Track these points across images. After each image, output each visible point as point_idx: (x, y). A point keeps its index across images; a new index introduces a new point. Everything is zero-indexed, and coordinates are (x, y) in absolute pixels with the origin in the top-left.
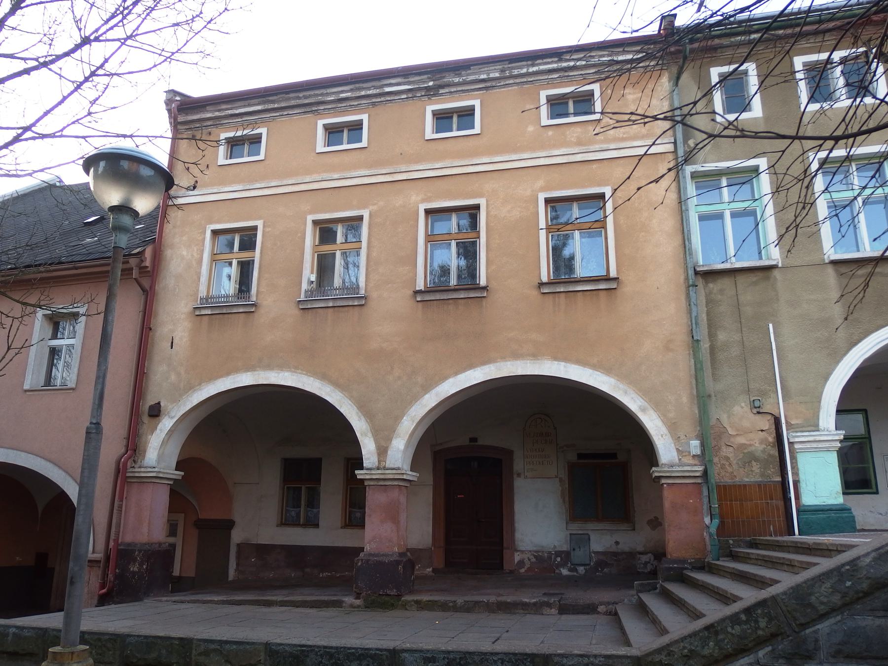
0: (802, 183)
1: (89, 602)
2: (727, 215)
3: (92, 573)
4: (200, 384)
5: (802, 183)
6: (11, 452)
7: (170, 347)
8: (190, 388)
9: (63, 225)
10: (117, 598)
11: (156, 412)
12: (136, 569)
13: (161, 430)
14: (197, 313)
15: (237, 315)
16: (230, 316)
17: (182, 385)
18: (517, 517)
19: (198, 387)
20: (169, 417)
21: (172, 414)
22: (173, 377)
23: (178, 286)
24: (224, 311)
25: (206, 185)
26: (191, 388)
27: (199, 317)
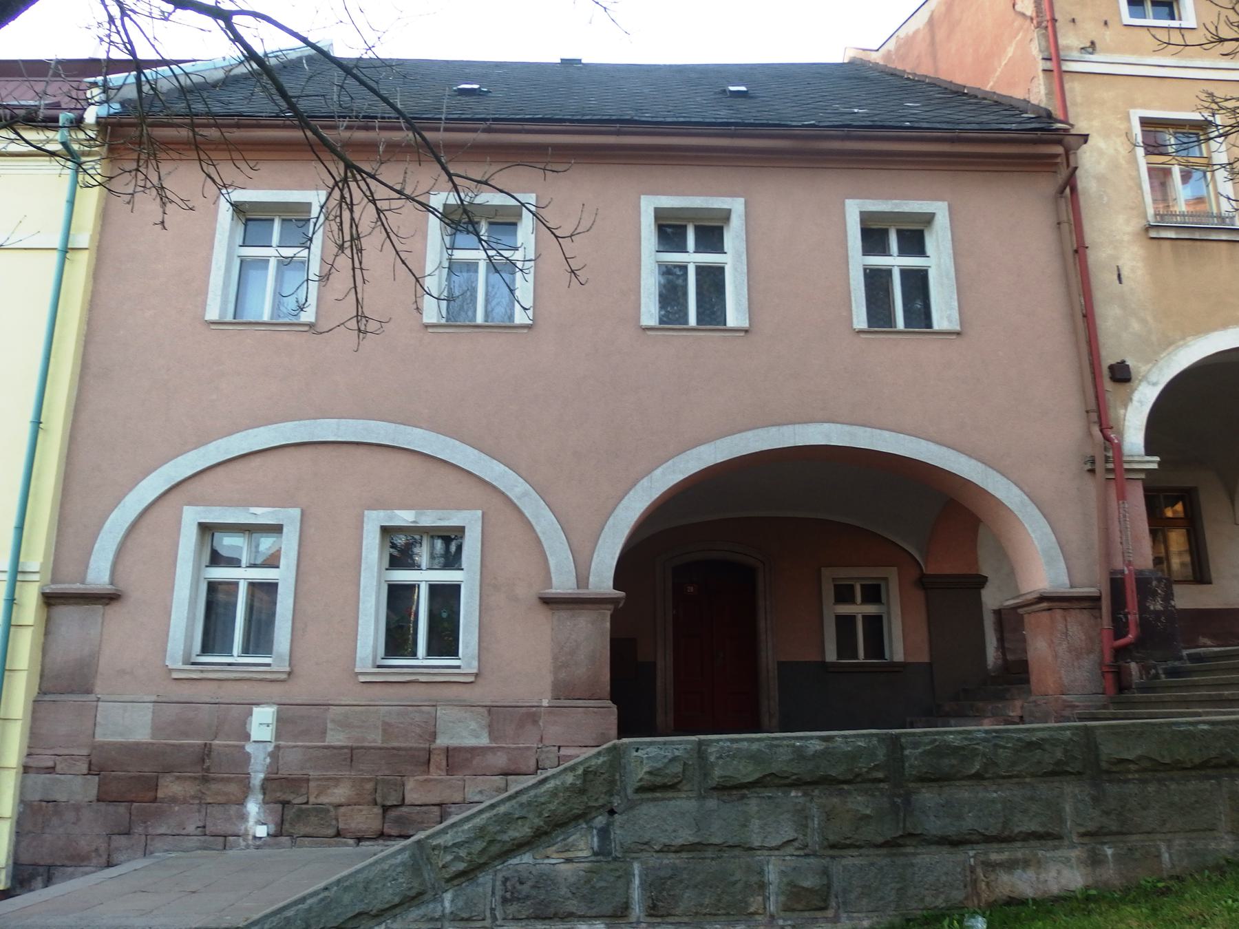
0: (576, 229)
1: (1076, 664)
2: (273, 264)
3: (1069, 619)
4: (1183, 338)
5: (576, 229)
6: (859, 431)
7: (1117, 282)
8: (1169, 343)
9: (490, 94)
10: (1138, 652)
11: (1122, 375)
12: (1159, 607)
13: (1140, 402)
14: (1153, 234)
15: (1215, 244)
16: (1205, 244)
17: (1154, 338)
18: (1207, 535)
19: (1181, 343)
20: (1149, 383)
21: (1153, 378)
22: (1136, 326)
23: (1104, 192)
24: (1197, 236)
25: (1108, 50)
26: (1170, 344)
27: (1155, 242)
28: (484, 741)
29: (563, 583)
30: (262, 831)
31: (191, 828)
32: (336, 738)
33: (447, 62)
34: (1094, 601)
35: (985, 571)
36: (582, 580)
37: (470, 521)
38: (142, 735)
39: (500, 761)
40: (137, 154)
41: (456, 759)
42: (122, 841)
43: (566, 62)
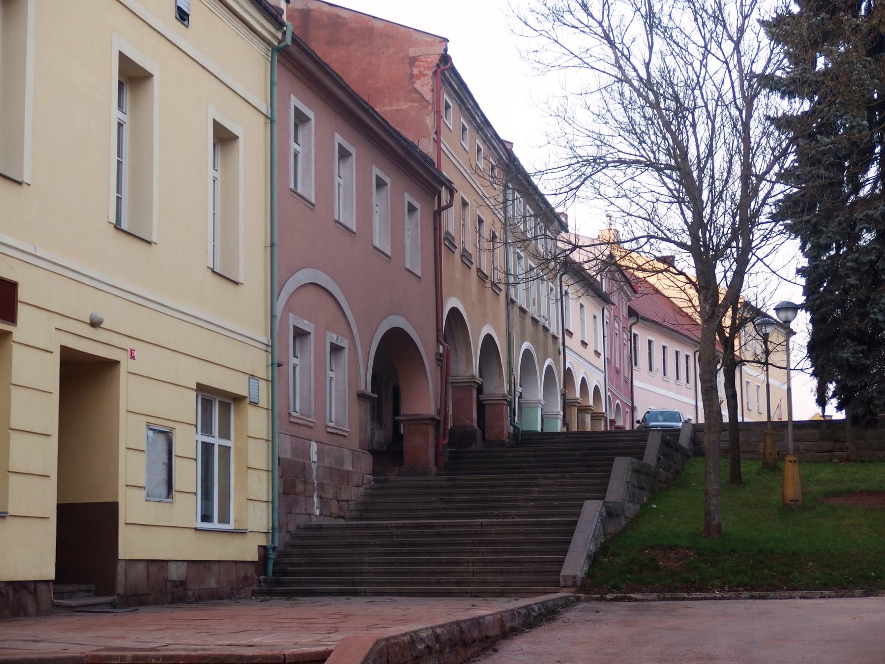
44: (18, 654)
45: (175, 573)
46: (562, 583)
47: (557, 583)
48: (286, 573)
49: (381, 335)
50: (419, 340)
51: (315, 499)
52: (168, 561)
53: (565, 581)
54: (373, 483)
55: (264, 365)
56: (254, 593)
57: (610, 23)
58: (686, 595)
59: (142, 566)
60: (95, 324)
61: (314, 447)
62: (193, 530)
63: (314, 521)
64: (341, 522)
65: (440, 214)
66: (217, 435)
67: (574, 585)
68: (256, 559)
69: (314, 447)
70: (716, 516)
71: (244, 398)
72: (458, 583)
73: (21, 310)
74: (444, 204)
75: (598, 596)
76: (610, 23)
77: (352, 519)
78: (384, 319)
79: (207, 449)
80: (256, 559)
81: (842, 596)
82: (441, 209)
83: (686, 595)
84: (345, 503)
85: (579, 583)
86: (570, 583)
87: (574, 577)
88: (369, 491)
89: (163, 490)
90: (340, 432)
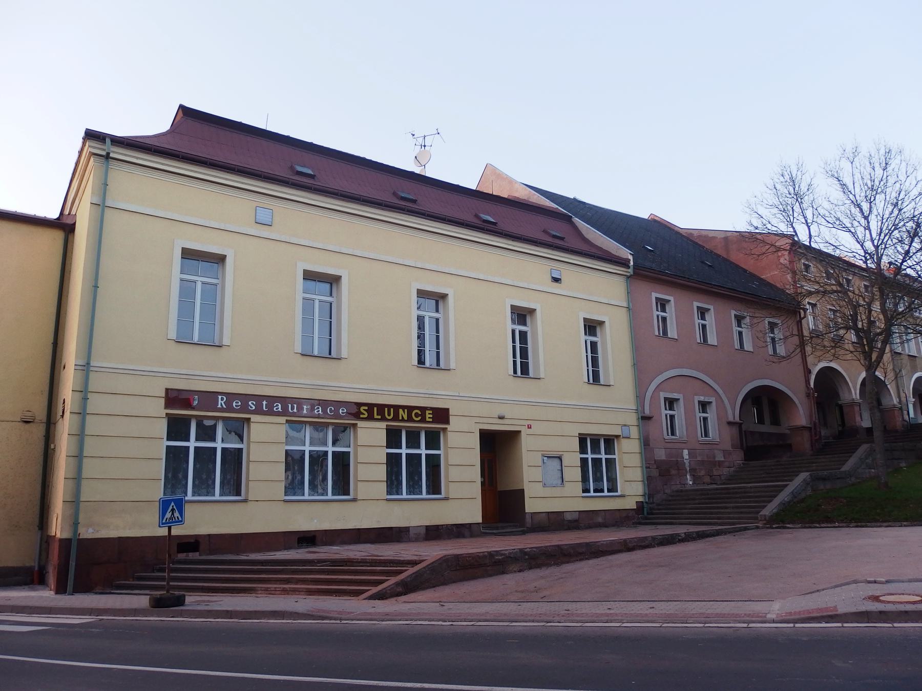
28: (723, 459)
29: (731, 419)
30: (691, 483)
31: (678, 483)
32: (699, 458)
33: (562, 196)
34: (810, 428)
35: (88, 397)
36: (734, 418)
37: (662, 395)
38: (664, 458)
39: (727, 464)
40: (797, 334)
41: (720, 464)
42: (665, 487)
43: (575, 199)
44: (403, 557)
45: (568, 517)
46: (759, 518)
47: (756, 518)
48: (652, 514)
49: (747, 392)
50: (786, 389)
51: (688, 477)
52: (563, 512)
53: (761, 518)
54: (742, 465)
55: (635, 419)
56: (633, 523)
57: (809, 229)
58: (818, 525)
59: (544, 514)
60: (501, 418)
61: (686, 452)
62: (581, 498)
63: (688, 487)
64: (715, 486)
65: (801, 322)
66: (604, 453)
67: (765, 519)
68: (636, 508)
69: (686, 452)
70: (882, 478)
71: (620, 436)
72: (719, 518)
73: (451, 418)
74: (802, 316)
75: (769, 526)
76: (809, 229)
77: (721, 484)
78: (750, 382)
79: (584, 461)
80: (636, 508)
81: (915, 525)
82: (801, 319)
83: (818, 525)
84: (718, 477)
85: (767, 518)
86: (763, 519)
87: (765, 515)
88: (738, 469)
89: (560, 481)
90: (711, 443)
